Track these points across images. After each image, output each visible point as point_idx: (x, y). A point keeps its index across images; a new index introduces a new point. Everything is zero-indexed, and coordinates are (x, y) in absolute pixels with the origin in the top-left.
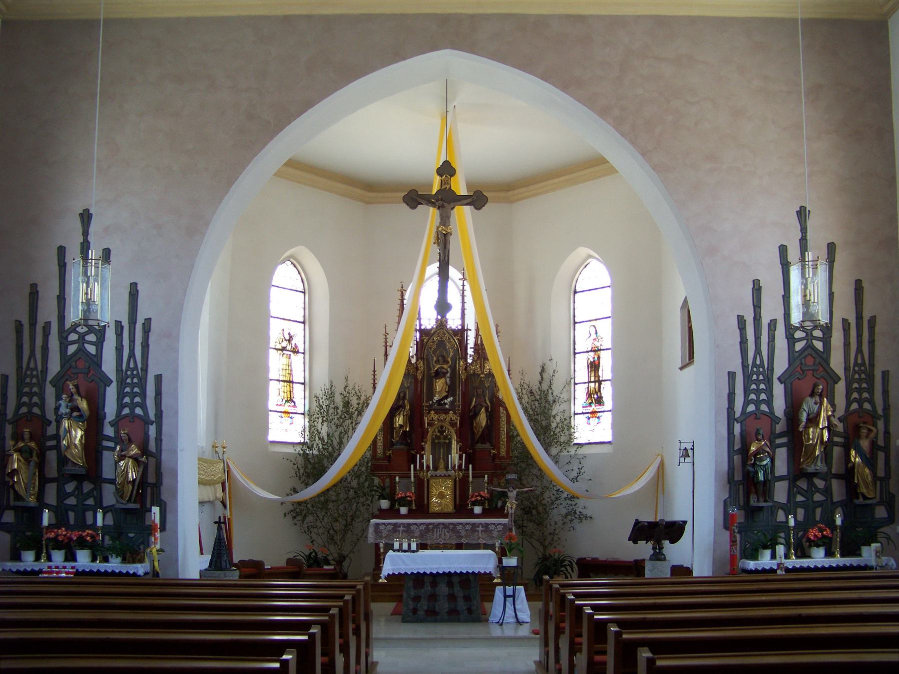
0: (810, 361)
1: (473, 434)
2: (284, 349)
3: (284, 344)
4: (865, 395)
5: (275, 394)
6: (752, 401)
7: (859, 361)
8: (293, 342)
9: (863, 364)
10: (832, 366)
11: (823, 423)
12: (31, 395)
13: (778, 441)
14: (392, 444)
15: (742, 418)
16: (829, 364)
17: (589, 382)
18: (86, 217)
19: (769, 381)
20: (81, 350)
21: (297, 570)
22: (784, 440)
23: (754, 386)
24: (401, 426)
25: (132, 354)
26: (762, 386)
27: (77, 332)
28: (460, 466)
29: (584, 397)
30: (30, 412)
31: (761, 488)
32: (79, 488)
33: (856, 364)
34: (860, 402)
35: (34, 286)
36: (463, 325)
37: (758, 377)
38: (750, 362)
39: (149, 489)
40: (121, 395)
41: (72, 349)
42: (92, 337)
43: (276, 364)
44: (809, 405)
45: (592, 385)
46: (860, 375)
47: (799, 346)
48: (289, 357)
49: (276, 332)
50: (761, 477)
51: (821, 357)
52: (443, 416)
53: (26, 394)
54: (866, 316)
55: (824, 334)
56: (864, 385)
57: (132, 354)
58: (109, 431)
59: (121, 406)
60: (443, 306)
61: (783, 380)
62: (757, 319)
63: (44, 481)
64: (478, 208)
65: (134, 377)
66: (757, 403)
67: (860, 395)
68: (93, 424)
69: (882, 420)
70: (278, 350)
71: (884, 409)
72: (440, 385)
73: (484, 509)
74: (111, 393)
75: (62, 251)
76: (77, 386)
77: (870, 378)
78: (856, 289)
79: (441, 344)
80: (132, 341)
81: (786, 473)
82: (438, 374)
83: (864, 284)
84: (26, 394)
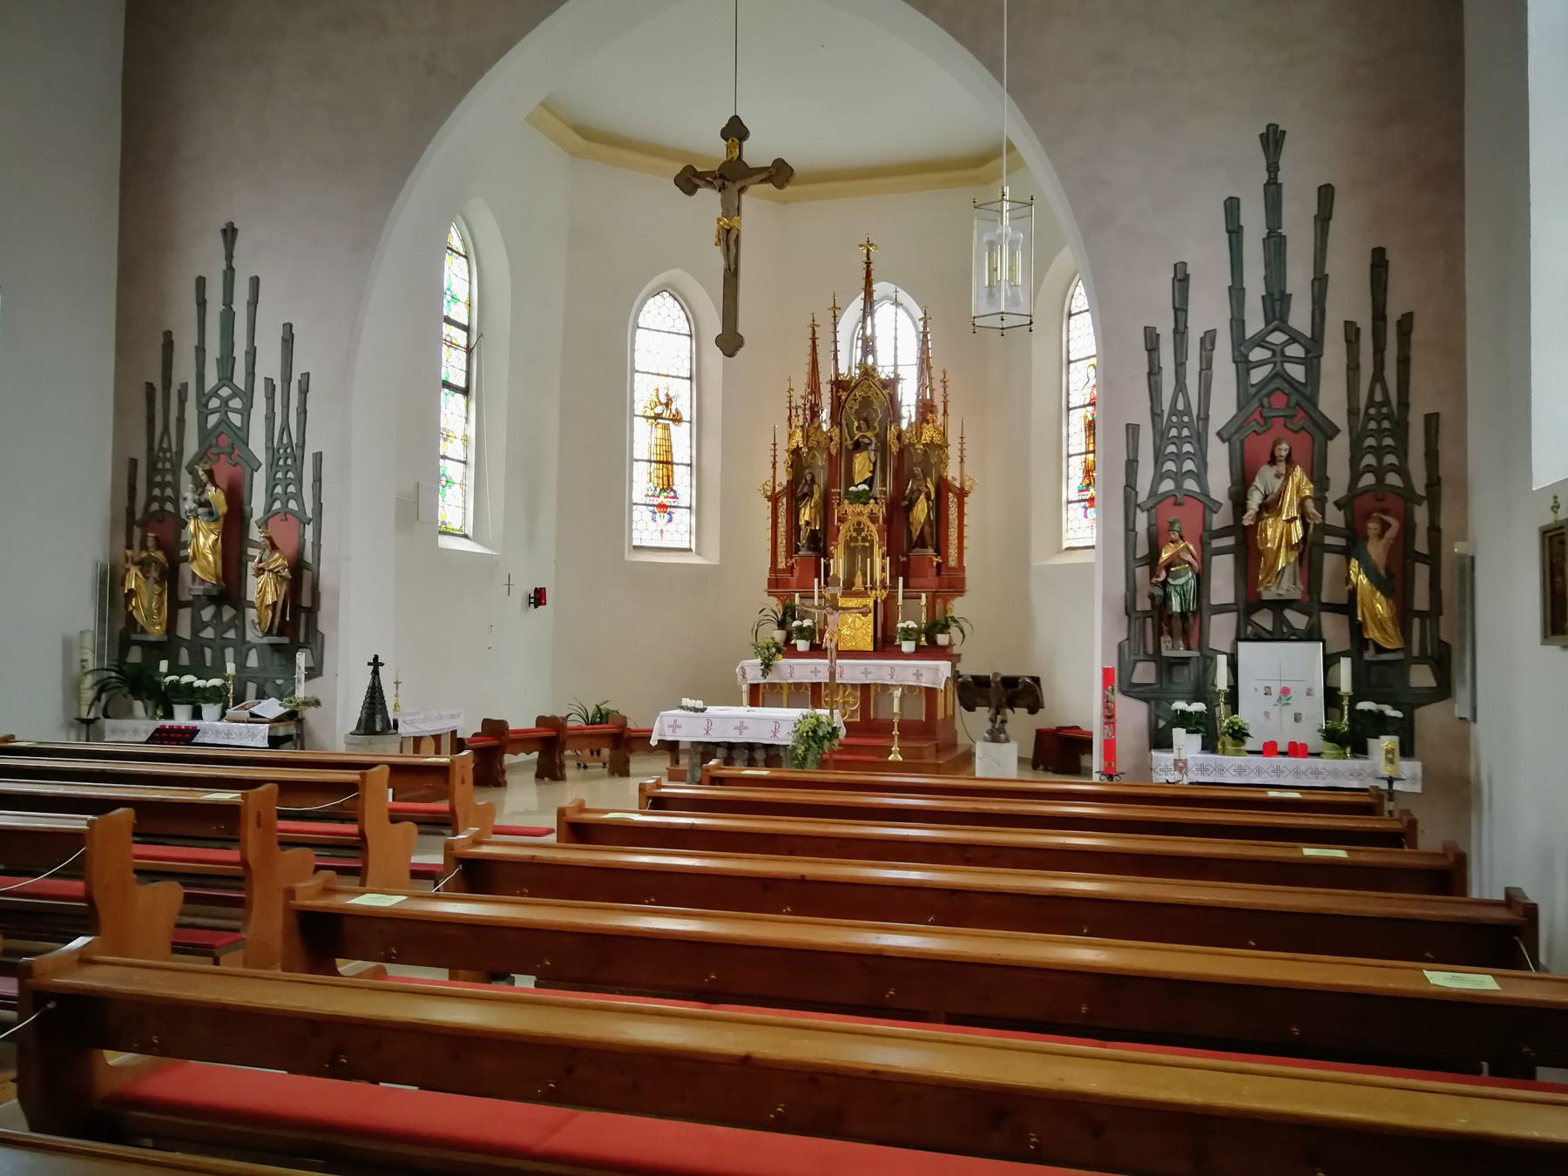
0: (1279, 400)
1: (910, 532)
2: (657, 417)
3: (659, 410)
4: (1390, 459)
5: (642, 481)
6: (1168, 474)
7: (1378, 397)
8: (673, 407)
9: (1386, 402)
10: (1322, 407)
11: (1289, 508)
12: (163, 485)
13: (1216, 543)
14: (797, 550)
15: (1151, 504)
16: (1315, 405)
17: (1087, 452)
18: (230, 233)
19: (1200, 439)
20: (224, 421)
21: (553, 733)
22: (1229, 541)
23: (1172, 449)
24: (808, 523)
25: (285, 427)
26: (1187, 448)
27: (219, 397)
28: (883, 581)
29: (1080, 474)
30: (162, 509)
31: (1177, 624)
32: (218, 614)
33: (1371, 402)
34: (1380, 472)
35: (168, 335)
36: (895, 372)
37: (1180, 432)
38: (1166, 407)
39: (303, 616)
40: (271, 483)
41: (213, 420)
42: (236, 403)
43: (644, 438)
44: (1266, 480)
45: (1091, 457)
46: (1379, 423)
47: (1257, 376)
48: (666, 428)
49: (644, 393)
50: (1176, 606)
51: (1301, 393)
52: (859, 508)
53: (159, 485)
54: (1394, 312)
55: (1307, 352)
56: (1388, 441)
57: (285, 427)
58: (255, 534)
59: (271, 497)
60: (868, 346)
61: (1225, 436)
62: (1180, 332)
63: (175, 605)
64: (780, 186)
65: (288, 456)
66: (1178, 477)
67: (1380, 460)
68: (234, 524)
69: (1425, 504)
70: (648, 418)
71: (1429, 486)
72: (862, 465)
73: (918, 646)
74: (260, 480)
75: (201, 283)
76: (210, 473)
77: (1400, 429)
78: (1373, 266)
79: (866, 402)
80: (286, 406)
81: (1232, 601)
82: (858, 446)
83: (1391, 256)
84: (159, 485)
